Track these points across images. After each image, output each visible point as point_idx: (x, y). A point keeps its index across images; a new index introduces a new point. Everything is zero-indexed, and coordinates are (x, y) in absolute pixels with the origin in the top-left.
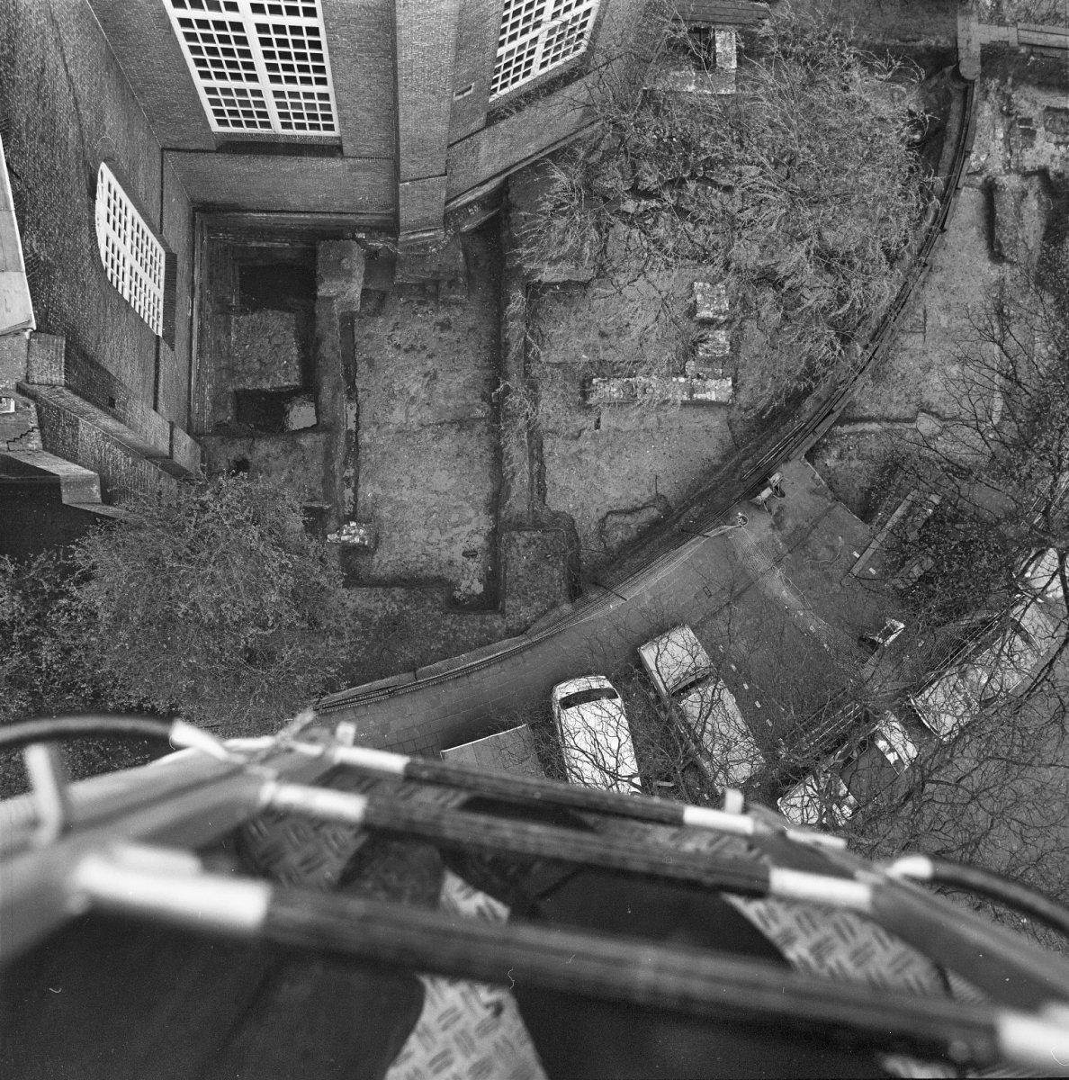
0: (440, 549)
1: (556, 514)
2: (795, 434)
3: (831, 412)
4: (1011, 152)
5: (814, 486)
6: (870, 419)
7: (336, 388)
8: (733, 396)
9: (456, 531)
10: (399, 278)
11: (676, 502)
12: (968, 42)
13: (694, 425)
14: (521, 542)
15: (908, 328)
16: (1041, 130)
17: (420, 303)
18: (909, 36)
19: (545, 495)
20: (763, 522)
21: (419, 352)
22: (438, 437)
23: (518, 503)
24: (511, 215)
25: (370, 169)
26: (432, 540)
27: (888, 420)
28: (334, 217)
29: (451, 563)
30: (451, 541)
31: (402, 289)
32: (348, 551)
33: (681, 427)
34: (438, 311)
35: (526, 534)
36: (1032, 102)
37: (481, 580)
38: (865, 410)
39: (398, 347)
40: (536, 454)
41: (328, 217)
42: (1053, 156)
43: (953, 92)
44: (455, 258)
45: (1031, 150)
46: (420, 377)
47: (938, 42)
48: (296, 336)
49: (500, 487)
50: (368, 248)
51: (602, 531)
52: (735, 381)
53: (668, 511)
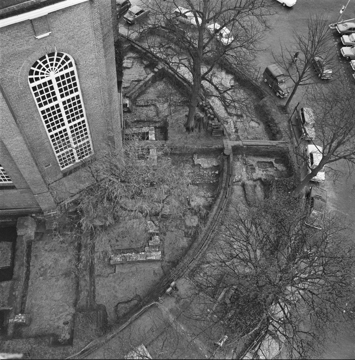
0: (55, 322)
1: (99, 306)
8: (162, 258)
9: (61, 315)
12: (227, 146)
16: (257, 168)
18: (209, 146)
23: (82, 302)
25: (27, 192)
26: (52, 319)
28: (24, 210)
29: (58, 327)
30: (59, 319)
32: (18, 326)
36: (253, 161)
37: (69, 334)
39: (46, 250)
40: (93, 284)
41: (21, 210)
42: (262, 175)
43: (224, 159)
44: (65, 219)
45: (255, 173)
47: (218, 146)
48: (11, 249)
50: (38, 219)
51: (116, 311)
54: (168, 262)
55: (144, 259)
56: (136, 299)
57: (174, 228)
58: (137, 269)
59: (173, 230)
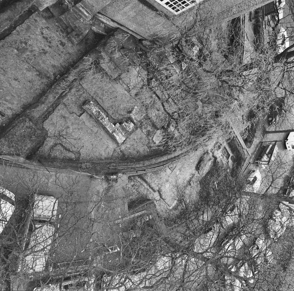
2: (132, 168)
3: (145, 170)
4: (214, 148)
5: (125, 187)
6: (146, 182)
7: (10, 19)
9: (4, 102)
10: (62, 17)
11: (82, 158)
13: (105, 141)
14: (27, 124)
15: (170, 167)
17: (61, 30)
19: (46, 120)
20: (105, 185)
21: (47, 42)
22: (28, 70)
23: (37, 113)
24: (111, 37)
27: (150, 186)
31: (60, 21)
33: (102, 139)
34: (64, 38)
35: (31, 123)
38: (147, 179)
39: (42, 34)
46: (41, 49)
49: (34, 104)
52: (126, 139)
53: (78, 159)
54: (121, 151)
55: (110, 132)
56: (75, 154)
57: (146, 130)
58: (97, 132)
59: (144, 131)
